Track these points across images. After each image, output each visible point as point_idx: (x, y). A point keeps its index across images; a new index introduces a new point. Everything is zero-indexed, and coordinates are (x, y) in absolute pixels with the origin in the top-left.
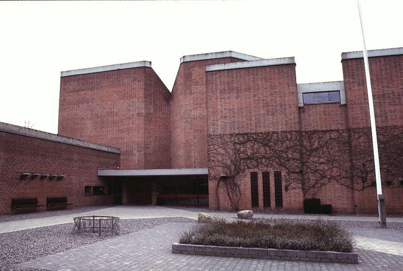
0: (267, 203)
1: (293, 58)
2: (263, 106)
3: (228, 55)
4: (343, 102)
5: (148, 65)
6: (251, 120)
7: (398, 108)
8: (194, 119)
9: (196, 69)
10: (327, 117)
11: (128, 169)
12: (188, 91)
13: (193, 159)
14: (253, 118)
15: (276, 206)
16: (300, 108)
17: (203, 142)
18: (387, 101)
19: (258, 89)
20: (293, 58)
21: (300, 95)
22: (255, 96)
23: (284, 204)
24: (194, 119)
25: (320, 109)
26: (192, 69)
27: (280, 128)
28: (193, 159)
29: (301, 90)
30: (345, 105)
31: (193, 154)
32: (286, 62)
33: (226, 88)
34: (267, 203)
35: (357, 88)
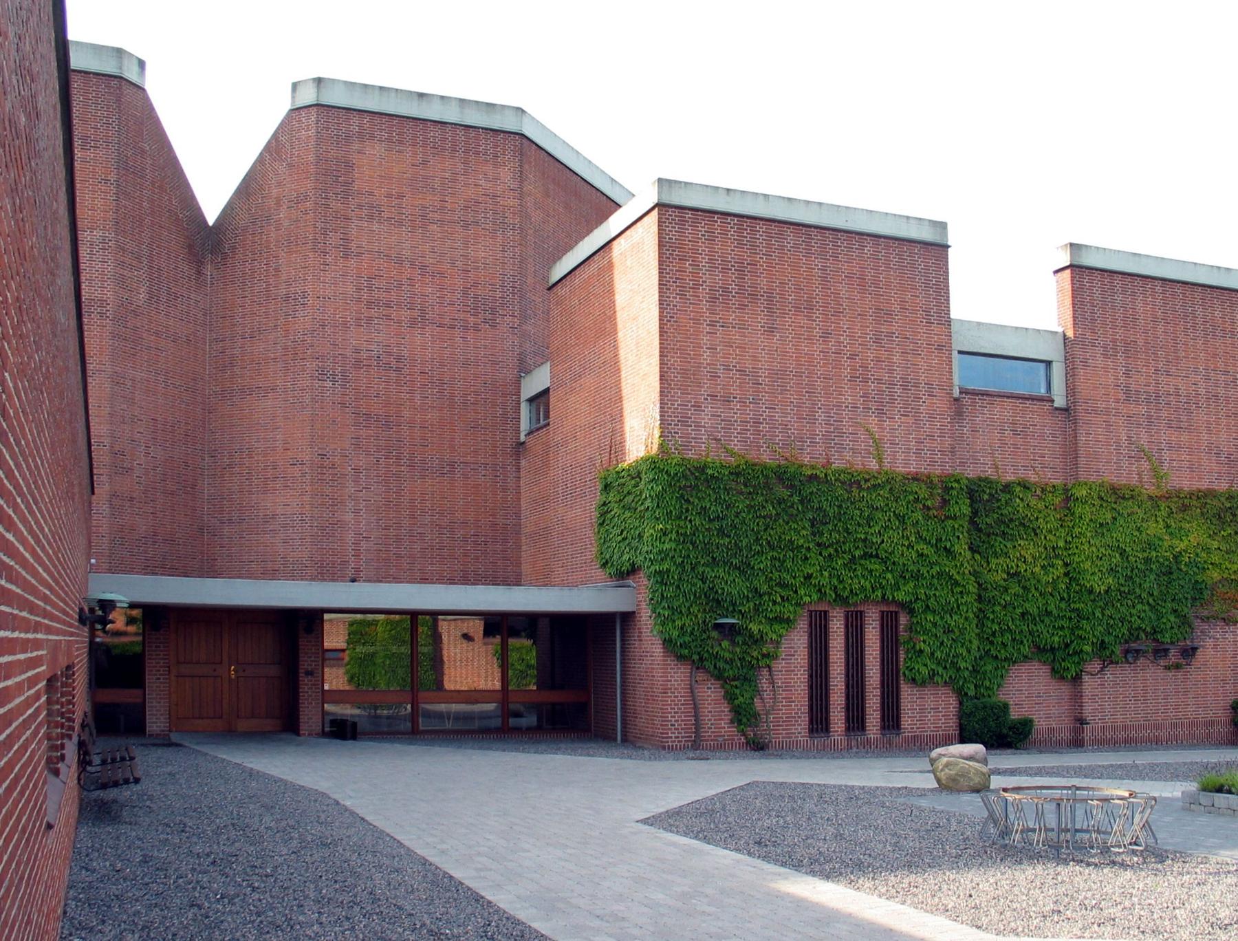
0: (856, 721)
1: (942, 226)
2: (853, 378)
3: (509, 124)
4: (1060, 402)
5: (132, 74)
6: (813, 422)
7: (1185, 437)
8: (358, 365)
9: (376, 150)
10: (1019, 440)
11: (271, 574)
12: (334, 239)
13: (350, 538)
14: (820, 416)
15: (883, 728)
16: (956, 400)
17: (394, 469)
18: (1164, 414)
19: (838, 313)
20: (942, 226)
21: (955, 354)
22: (826, 336)
23: (906, 722)
24: (358, 365)
25: (1004, 411)
26: (356, 146)
27: (902, 462)
28: (350, 538)
29: (961, 341)
30: (1066, 410)
31: (349, 517)
32: (926, 235)
33: (733, 288)
34: (856, 721)
35: (1100, 361)
